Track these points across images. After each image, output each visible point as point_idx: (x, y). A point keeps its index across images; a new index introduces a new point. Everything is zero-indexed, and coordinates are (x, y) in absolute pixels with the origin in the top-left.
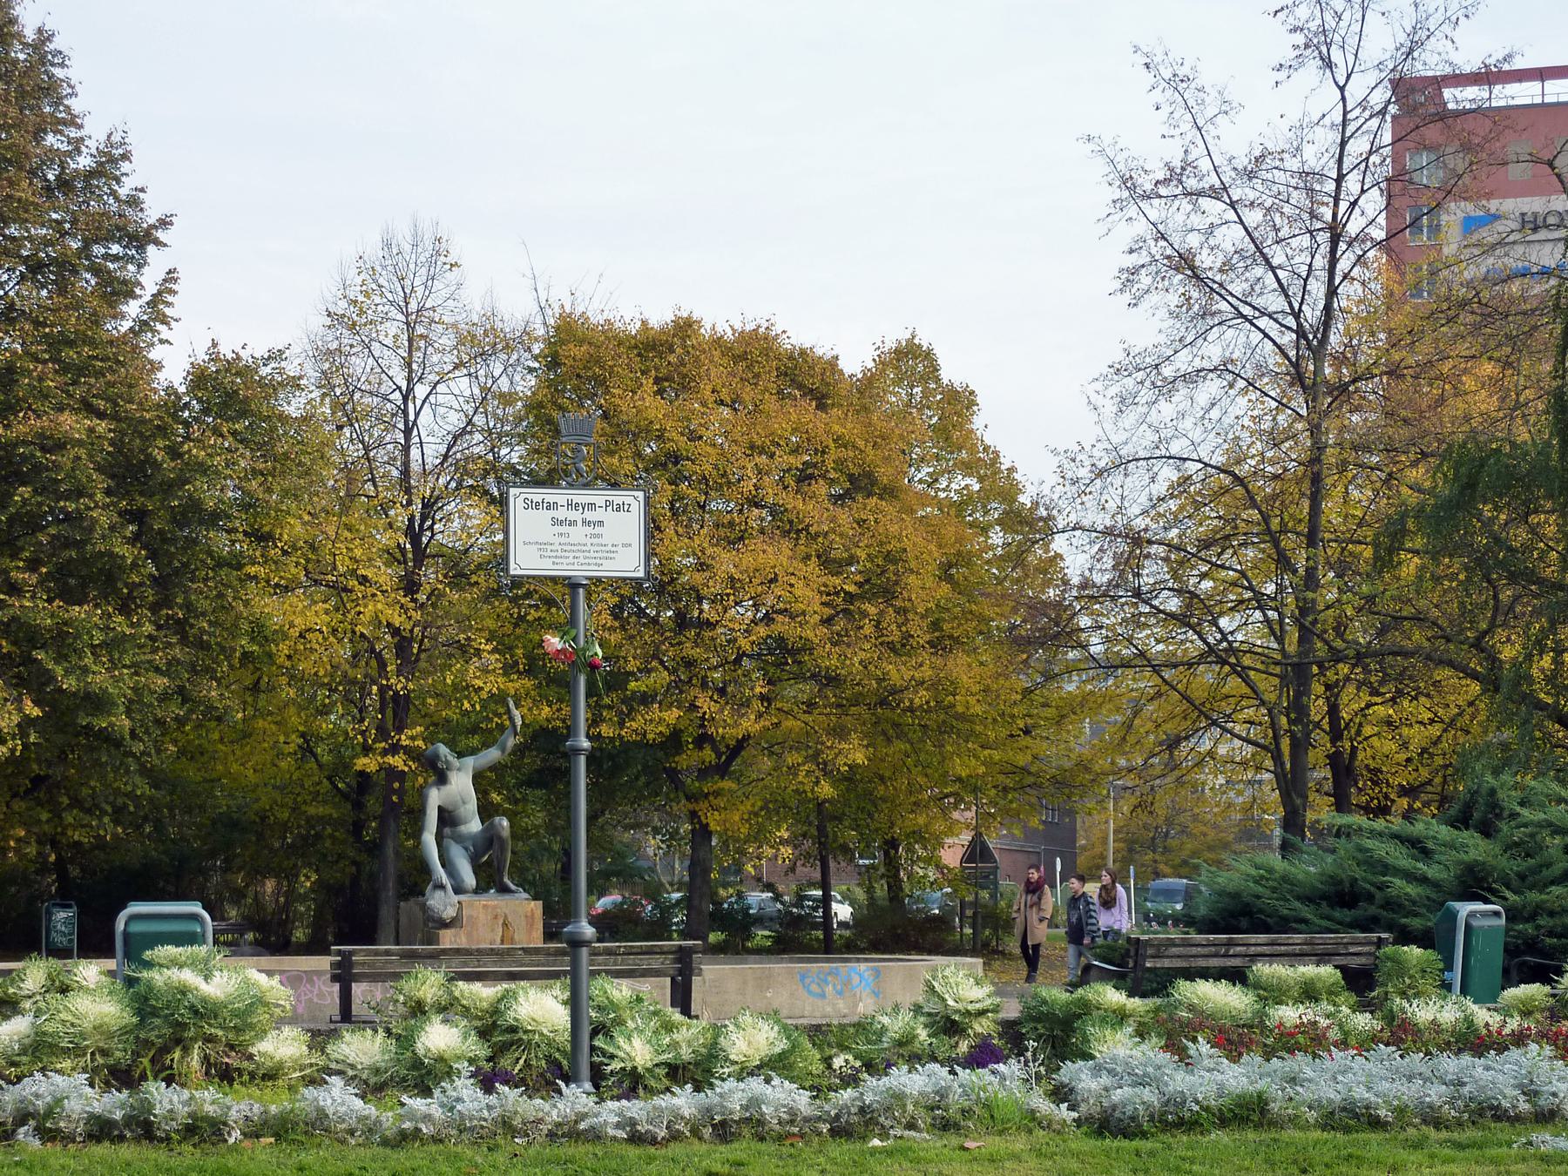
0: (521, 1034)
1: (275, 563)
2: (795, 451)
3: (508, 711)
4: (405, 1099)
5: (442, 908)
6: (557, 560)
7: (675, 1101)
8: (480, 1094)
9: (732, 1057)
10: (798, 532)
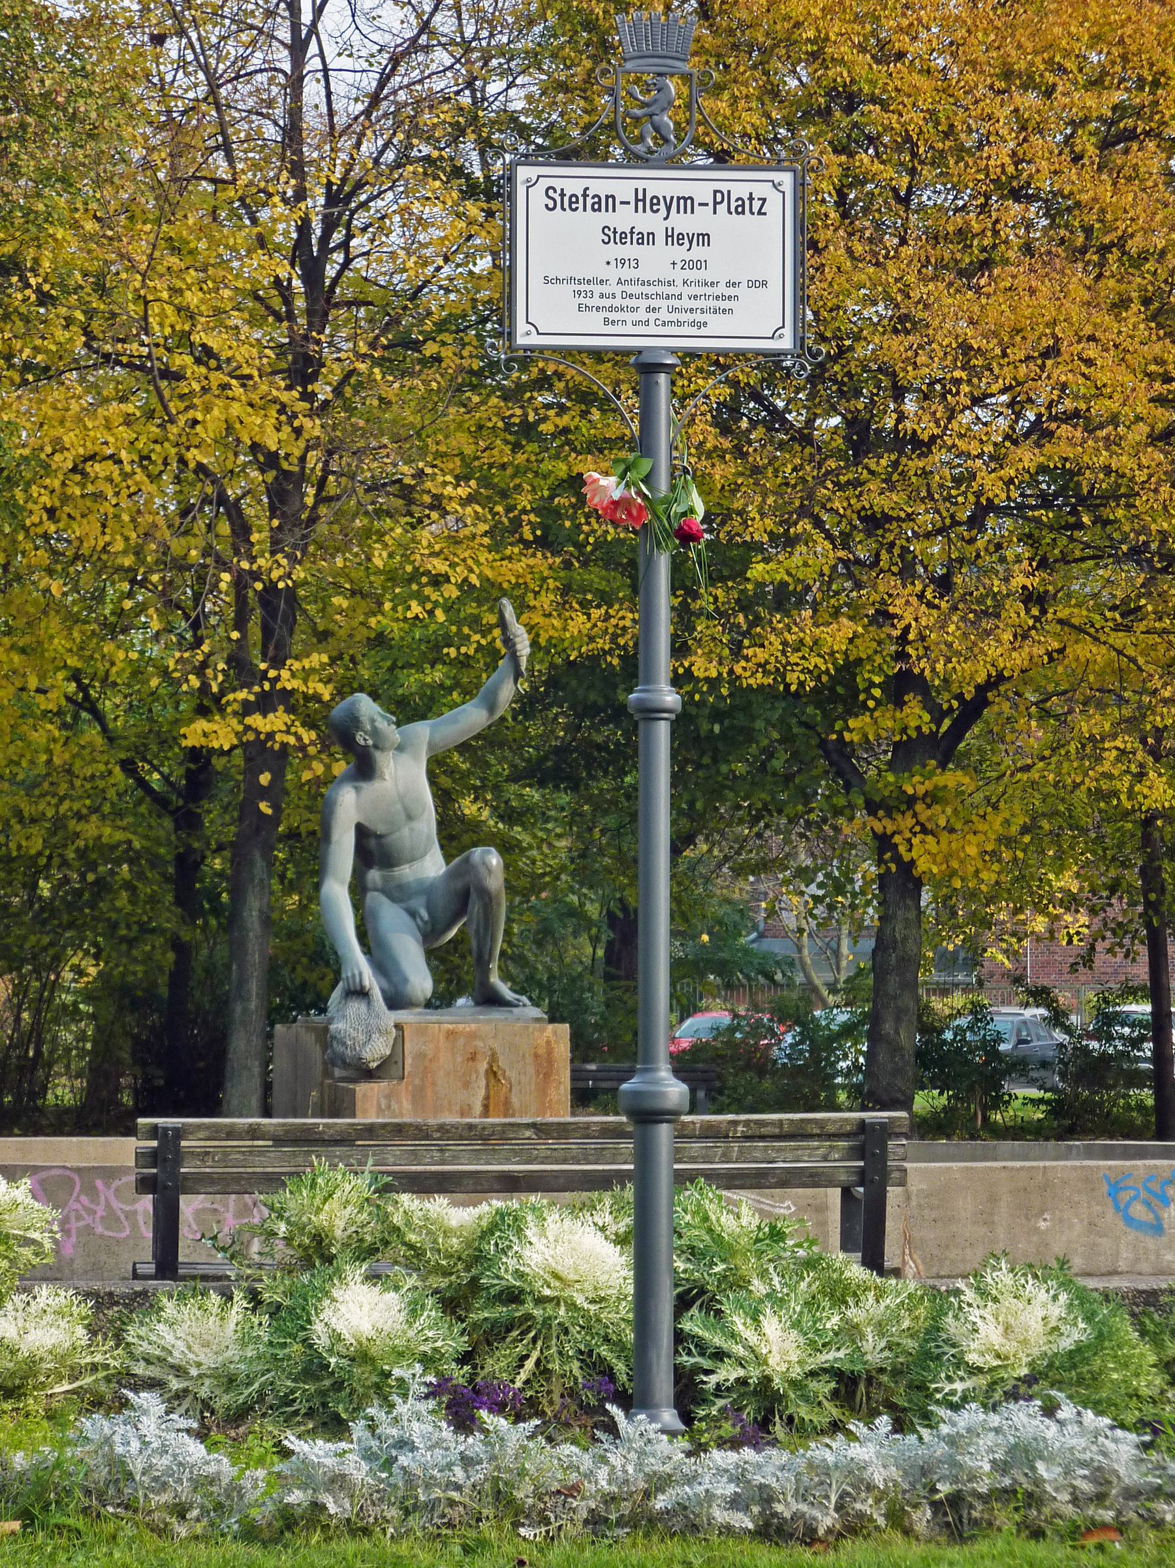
0: (529, 1307)
1: (26, 320)
2: (1096, 83)
3: (502, 624)
4: (292, 1442)
5: (362, 1038)
6: (613, 316)
7: (857, 1452)
8: (447, 1432)
9: (972, 1358)
10: (1104, 249)
